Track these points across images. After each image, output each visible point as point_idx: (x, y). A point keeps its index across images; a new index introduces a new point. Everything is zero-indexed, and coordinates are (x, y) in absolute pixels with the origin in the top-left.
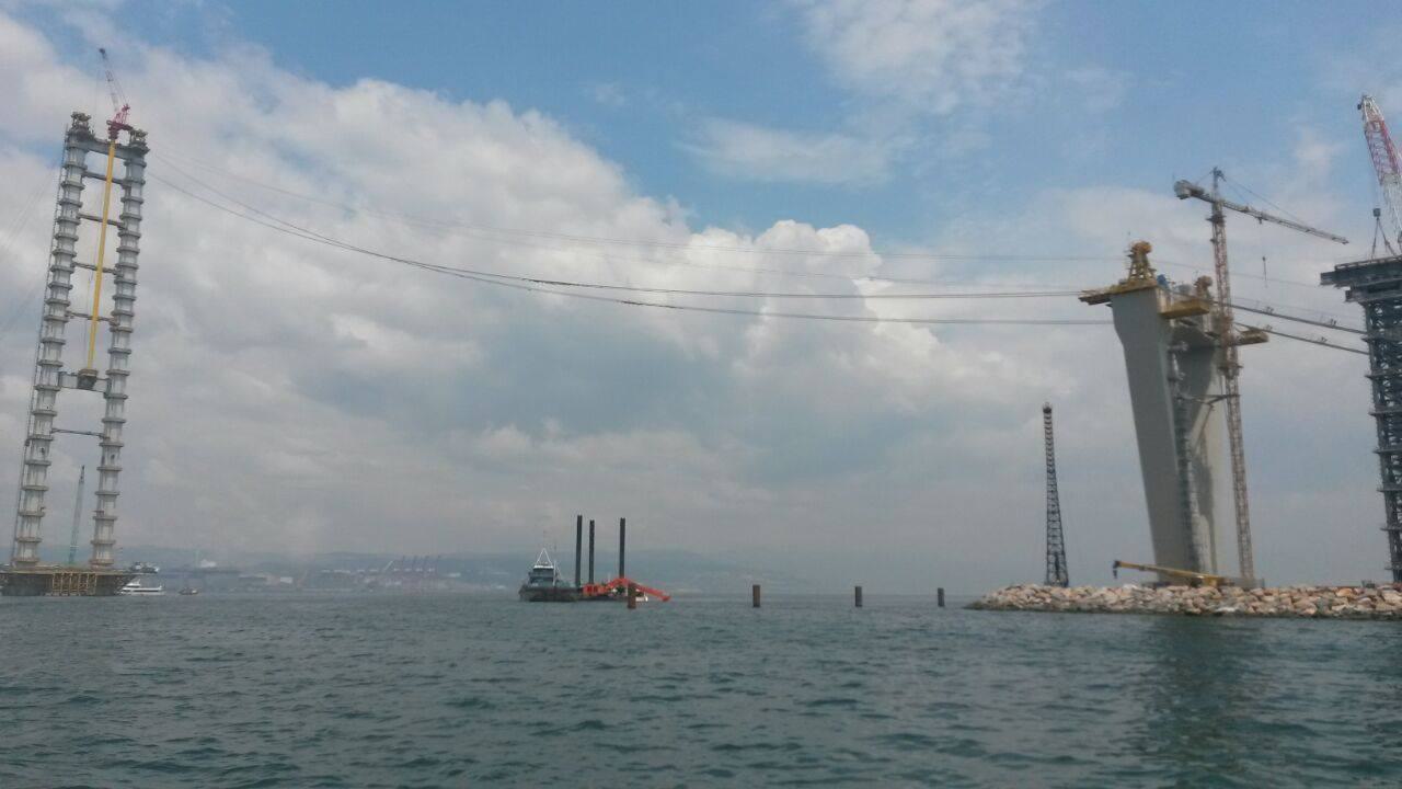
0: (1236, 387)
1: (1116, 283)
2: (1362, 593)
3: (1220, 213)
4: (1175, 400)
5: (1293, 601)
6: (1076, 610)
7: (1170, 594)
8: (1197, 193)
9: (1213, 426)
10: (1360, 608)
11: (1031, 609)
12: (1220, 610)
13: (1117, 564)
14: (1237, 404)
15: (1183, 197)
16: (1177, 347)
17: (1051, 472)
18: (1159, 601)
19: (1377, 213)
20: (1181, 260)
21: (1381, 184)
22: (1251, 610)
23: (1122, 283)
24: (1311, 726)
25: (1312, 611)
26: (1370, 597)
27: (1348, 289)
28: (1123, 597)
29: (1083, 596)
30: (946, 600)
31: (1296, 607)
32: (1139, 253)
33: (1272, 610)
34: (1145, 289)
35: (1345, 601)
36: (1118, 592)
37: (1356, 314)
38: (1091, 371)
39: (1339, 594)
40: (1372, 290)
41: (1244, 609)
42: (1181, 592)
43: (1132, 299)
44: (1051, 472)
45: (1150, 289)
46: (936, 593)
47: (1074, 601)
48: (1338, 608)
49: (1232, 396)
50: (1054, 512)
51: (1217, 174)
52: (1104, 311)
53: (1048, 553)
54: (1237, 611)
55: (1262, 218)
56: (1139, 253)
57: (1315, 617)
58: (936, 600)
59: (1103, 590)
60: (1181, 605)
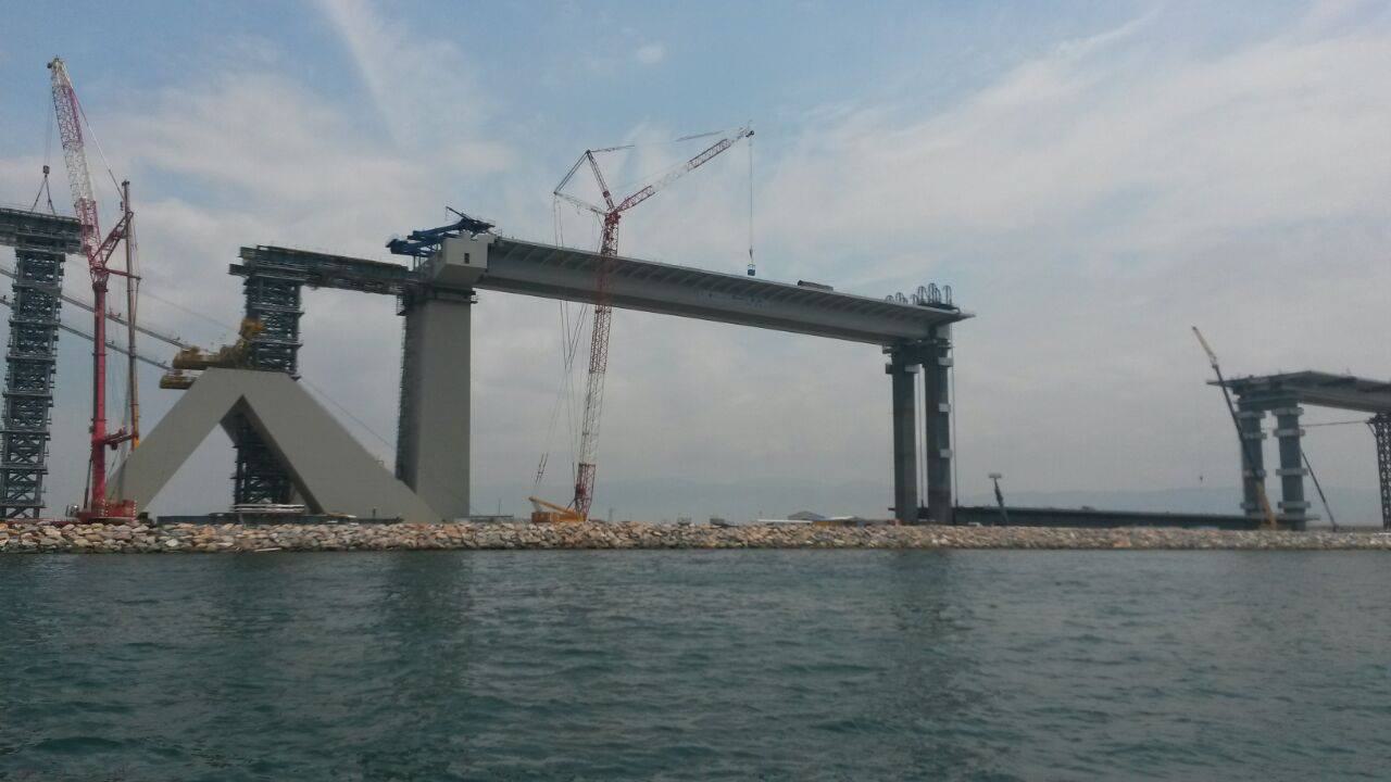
2: (22, 528)
10: (25, 542)
19: (46, 170)
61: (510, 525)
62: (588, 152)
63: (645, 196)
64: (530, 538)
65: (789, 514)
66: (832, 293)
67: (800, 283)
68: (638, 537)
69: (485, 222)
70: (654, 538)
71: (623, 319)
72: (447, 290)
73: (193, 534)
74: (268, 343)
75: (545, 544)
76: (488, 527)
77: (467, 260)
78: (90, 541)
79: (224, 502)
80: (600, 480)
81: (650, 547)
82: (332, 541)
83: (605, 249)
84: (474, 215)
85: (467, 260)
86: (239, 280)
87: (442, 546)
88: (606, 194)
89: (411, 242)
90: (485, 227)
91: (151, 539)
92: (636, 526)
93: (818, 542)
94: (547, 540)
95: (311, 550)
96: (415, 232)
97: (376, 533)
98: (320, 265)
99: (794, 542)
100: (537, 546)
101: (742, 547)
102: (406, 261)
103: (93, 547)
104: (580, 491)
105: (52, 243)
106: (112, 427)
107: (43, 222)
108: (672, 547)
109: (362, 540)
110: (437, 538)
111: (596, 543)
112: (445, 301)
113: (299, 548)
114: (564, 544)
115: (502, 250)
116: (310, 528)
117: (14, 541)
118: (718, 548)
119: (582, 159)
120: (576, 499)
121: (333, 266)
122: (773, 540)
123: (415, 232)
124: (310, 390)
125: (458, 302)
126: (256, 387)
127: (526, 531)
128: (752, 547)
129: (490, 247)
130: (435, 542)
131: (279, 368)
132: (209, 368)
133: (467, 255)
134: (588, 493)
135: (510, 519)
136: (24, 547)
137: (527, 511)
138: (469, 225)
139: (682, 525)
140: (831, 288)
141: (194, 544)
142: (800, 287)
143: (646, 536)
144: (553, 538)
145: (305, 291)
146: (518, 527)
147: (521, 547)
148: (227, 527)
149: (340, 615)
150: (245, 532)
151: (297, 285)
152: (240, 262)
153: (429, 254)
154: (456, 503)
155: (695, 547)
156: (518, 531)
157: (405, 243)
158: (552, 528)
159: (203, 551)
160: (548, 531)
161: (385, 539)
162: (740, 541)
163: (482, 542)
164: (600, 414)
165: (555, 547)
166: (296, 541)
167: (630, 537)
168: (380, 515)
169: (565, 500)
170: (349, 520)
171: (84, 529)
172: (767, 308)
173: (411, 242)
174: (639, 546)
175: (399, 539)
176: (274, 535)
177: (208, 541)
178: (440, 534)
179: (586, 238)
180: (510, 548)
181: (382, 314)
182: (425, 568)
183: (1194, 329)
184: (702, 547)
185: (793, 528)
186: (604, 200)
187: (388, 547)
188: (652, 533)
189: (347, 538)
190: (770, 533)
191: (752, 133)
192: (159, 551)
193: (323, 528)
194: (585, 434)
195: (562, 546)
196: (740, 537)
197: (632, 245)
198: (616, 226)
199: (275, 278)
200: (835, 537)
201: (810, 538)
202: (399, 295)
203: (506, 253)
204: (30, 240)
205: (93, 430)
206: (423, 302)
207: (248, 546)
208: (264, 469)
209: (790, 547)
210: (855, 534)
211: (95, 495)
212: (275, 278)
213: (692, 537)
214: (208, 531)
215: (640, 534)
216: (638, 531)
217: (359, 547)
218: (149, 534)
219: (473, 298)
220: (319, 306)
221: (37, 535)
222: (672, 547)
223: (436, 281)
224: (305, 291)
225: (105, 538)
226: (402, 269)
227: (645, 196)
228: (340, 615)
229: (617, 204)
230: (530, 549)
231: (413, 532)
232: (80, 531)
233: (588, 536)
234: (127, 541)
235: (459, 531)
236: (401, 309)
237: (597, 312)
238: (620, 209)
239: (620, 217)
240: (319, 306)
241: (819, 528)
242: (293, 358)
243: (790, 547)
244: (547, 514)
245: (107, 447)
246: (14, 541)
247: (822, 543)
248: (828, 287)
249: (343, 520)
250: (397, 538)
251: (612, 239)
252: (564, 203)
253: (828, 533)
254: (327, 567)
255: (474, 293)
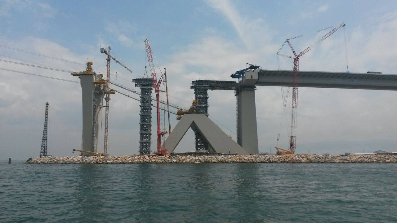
0: (108, 104)
1: (82, 71)
2: (141, 157)
3: (109, 59)
4: (94, 106)
5: (125, 160)
6: (49, 163)
7: (92, 158)
8: (105, 52)
9: (102, 113)
10: (141, 161)
11: (50, 164)
12: (107, 162)
13: (74, 150)
14: (108, 109)
15: (102, 52)
16: (96, 92)
17: (46, 122)
18: (89, 160)
19: (146, 67)
20: (99, 69)
21: (149, 61)
22: (115, 162)
23: (84, 72)
24: (279, 198)
25: (130, 162)
26: (142, 158)
27: (136, 84)
28: (79, 159)
29: (66, 159)
30: (12, 161)
31: (126, 161)
32: (89, 64)
33: (121, 162)
34: (90, 75)
35: (137, 159)
36: (77, 158)
37: (138, 90)
38: (75, 93)
39: (136, 157)
40: (143, 85)
41: (113, 161)
42: (95, 158)
43: (86, 76)
44: (46, 122)
45: (92, 75)
46: (8, 159)
47: (64, 161)
48: (136, 161)
49: (107, 106)
50: (45, 135)
51: (110, 48)
52: (77, 79)
53: (42, 147)
54: (112, 162)
55: (117, 62)
56: (89, 64)
57: (131, 163)
58: (8, 161)
59: (72, 158)
60: (96, 161)
61: (267, 156)
62: (287, 40)
63: (307, 51)
64: (274, 159)
65: (374, 151)
66: (381, 74)
67: (368, 72)
68: (310, 159)
69: (257, 66)
70: (316, 160)
71: (302, 91)
72: (248, 87)
73: (180, 158)
74: (200, 106)
75: (279, 161)
76: (260, 156)
77: (252, 78)
78: (155, 160)
79: (193, 150)
80: (298, 142)
81: (314, 163)
82: (215, 160)
83: (295, 69)
84: (255, 64)
85: (252, 78)
86: (193, 90)
87: (246, 162)
88: (294, 52)
89: (237, 74)
90: (258, 67)
91: (170, 159)
92: (310, 156)
93: (379, 161)
94: (279, 160)
95: (210, 162)
96: (237, 71)
97: (227, 158)
98: (212, 84)
99: (369, 161)
100: (276, 162)
101: (349, 163)
102: (237, 80)
103: (156, 162)
104: (292, 145)
105: (148, 85)
106: (161, 131)
107: (146, 80)
108: (322, 163)
109: (223, 160)
110: (245, 160)
111: (295, 161)
112: (247, 90)
113: (206, 162)
114: (285, 161)
115: (263, 74)
116: (210, 156)
117: (138, 160)
118: (339, 163)
119: (285, 43)
120: (290, 147)
121: (215, 84)
122: (361, 160)
123: (237, 71)
124: (211, 119)
125: (251, 90)
126: (197, 118)
127: (272, 157)
128: (352, 162)
129: (259, 73)
130: (244, 161)
131: (203, 113)
132: (185, 114)
133: (252, 76)
134: (294, 145)
135: (267, 154)
136: (141, 162)
137: (275, 152)
138: (252, 67)
139: (326, 155)
140: (381, 73)
141: (180, 161)
142: (369, 74)
143: (313, 159)
144: (281, 159)
145: (209, 91)
146: (270, 156)
147: (270, 162)
148: (188, 156)
149: (225, 182)
150: (193, 158)
151: (206, 90)
152: (192, 85)
153: (242, 77)
154: (254, 149)
155: (331, 163)
156: (270, 157)
157: (235, 75)
158: (281, 157)
159: (182, 163)
160: (280, 157)
161: (230, 160)
162: (348, 161)
163: (258, 161)
164: (296, 121)
165: (282, 162)
166: (206, 160)
167: (308, 159)
168: (231, 153)
169: (287, 148)
170: (221, 154)
171: (154, 157)
172: (356, 82)
173: (237, 74)
174: (311, 162)
175: (234, 160)
176: (200, 158)
177: (183, 160)
178: (246, 158)
179: (288, 67)
180: (267, 163)
181: (229, 97)
182: (248, 167)
183: (47, 104)
184: (333, 163)
185: (369, 156)
186: (293, 54)
187: (231, 162)
188: (315, 158)
189: (219, 159)
190: (360, 158)
191: (344, 25)
192: (171, 163)
193: (213, 156)
194: (292, 127)
195: (284, 162)
196: (348, 159)
197: (304, 66)
198: (298, 61)
199: (202, 88)
200: (386, 159)
201: (376, 159)
202: (235, 90)
203: (264, 74)
204: (143, 85)
205: (158, 132)
206: (241, 91)
207: (193, 162)
208: (202, 141)
209: (368, 162)
210: (395, 158)
211: (159, 148)
212: (202, 88)
213: (330, 159)
214: (184, 157)
215: (311, 158)
216: (310, 157)
217: (223, 162)
218: (169, 158)
219: (255, 88)
220: (213, 95)
221: (143, 159)
222: (322, 163)
223: (245, 85)
224: (209, 91)
225: (159, 159)
226: (234, 82)
227: (307, 51)
228: (225, 182)
229: (298, 55)
230: (273, 163)
231: (238, 158)
232: (153, 157)
233: (293, 159)
234: (164, 160)
235: (251, 157)
236: (236, 94)
237: (293, 89)
238: (299, 56)
239: (299, 58)
240: (213, 95)
241: (379, 156)
242: (206, 110)
243: (368, 162)
244: (281, 152)
245: (161, 136)
246: (138, 160)
247: (381, 161)
248: (379, 73)
249: (219, 154)
250: (233, 160)
251: (297, 66)
252: (280, 57)
253: (383, 158)
254: (217, 167)
255: (255, 87)
